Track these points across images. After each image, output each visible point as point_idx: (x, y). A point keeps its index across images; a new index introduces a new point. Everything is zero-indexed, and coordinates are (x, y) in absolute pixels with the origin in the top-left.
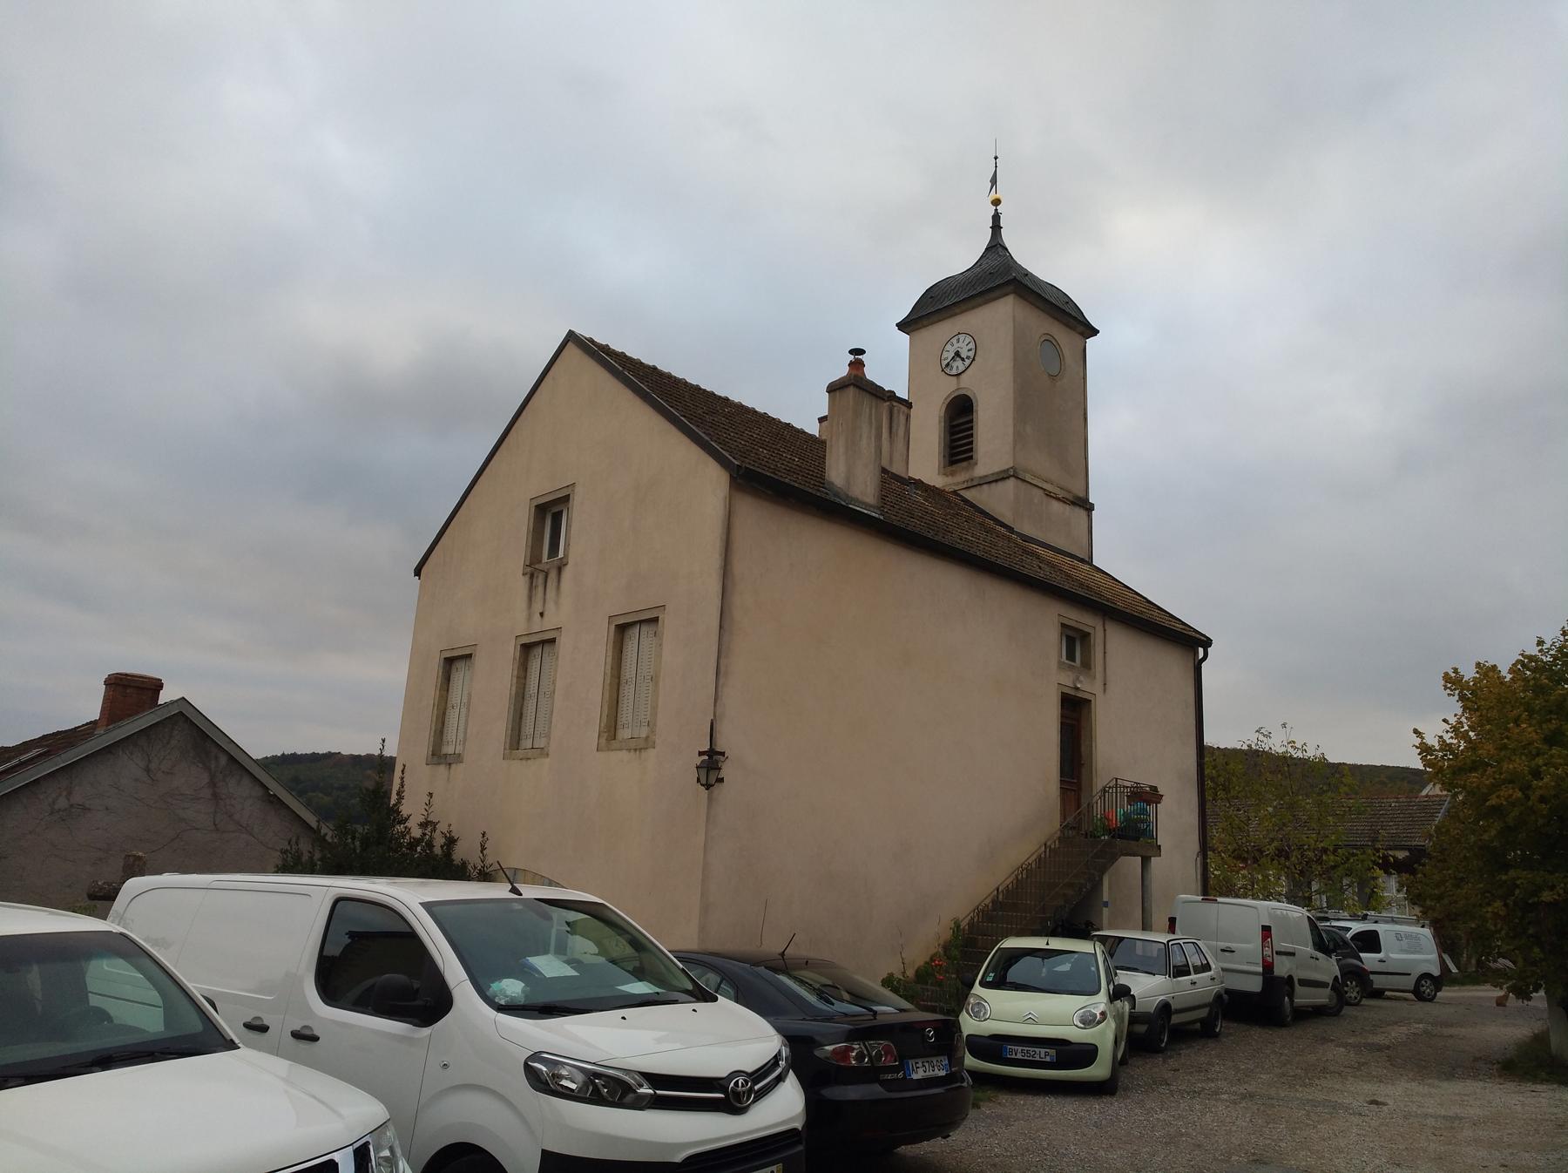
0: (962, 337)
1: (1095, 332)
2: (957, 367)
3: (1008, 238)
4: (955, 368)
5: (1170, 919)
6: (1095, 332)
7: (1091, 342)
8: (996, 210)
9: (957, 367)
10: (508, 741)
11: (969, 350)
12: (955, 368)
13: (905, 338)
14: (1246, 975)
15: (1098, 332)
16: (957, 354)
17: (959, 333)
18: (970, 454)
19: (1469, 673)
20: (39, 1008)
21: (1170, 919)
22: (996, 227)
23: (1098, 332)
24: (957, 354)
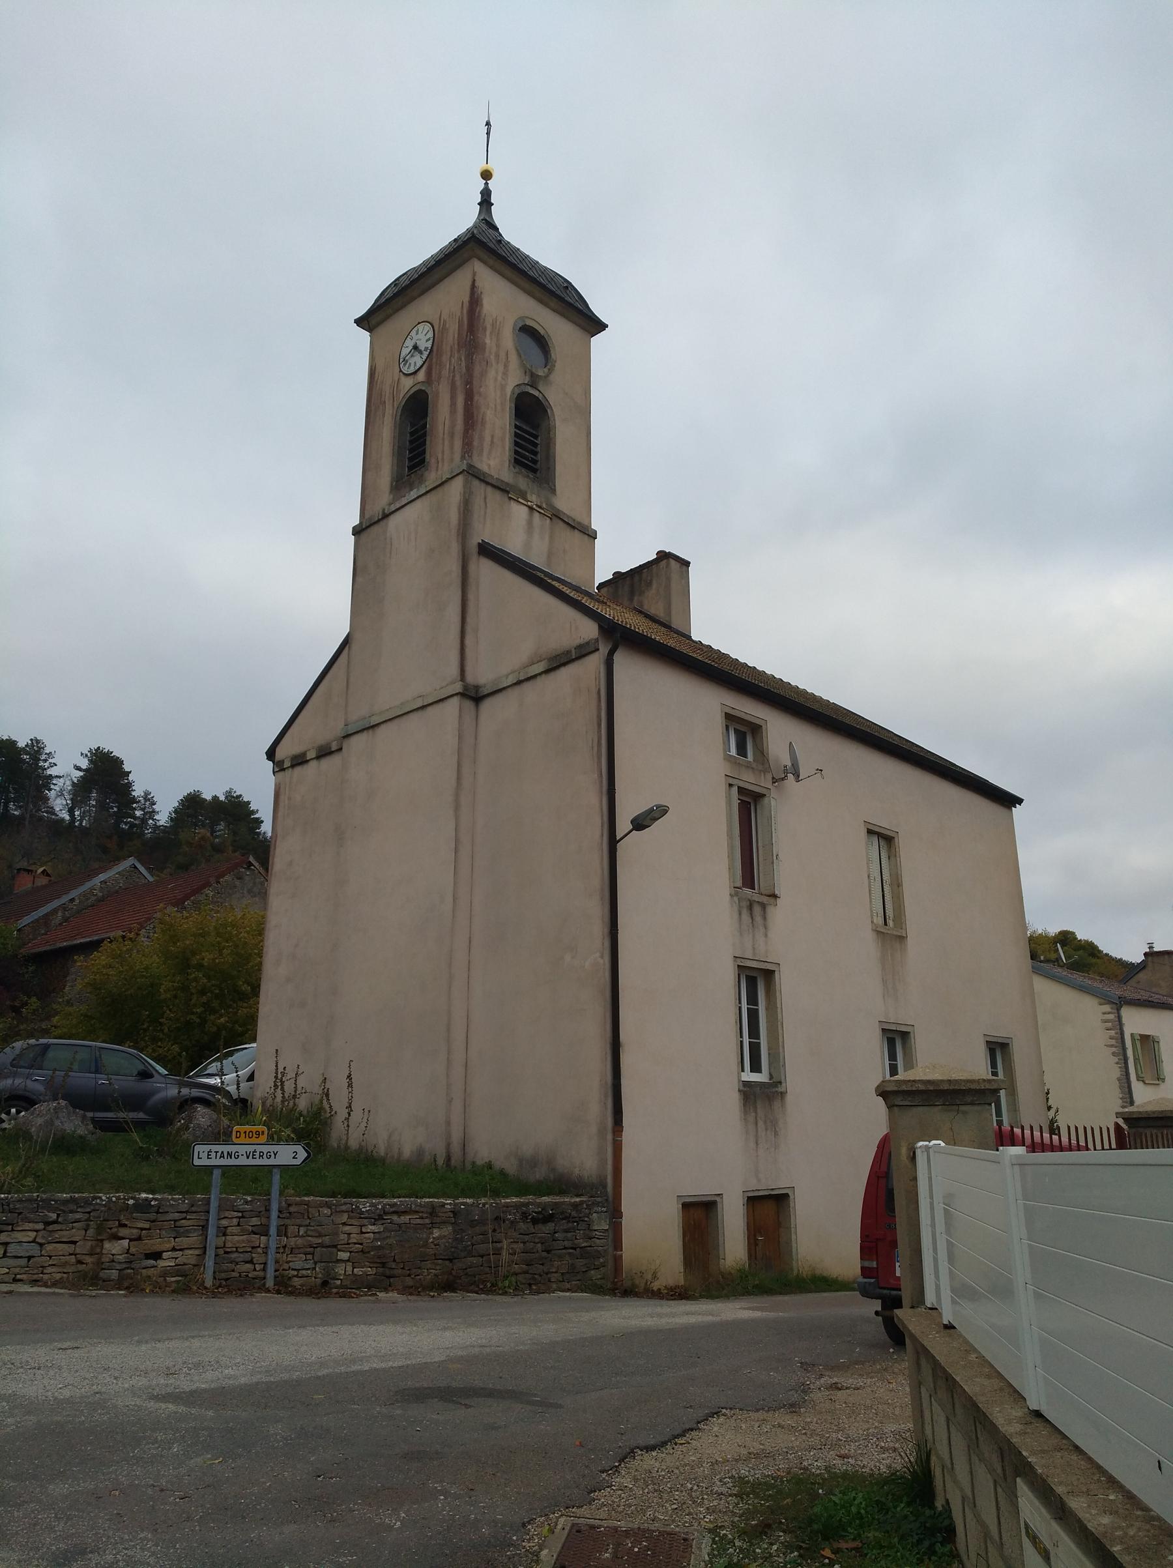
0: (420, 327)
1: (599, 326)
2: (415, 363)
3: (498, 216)
4: (412, 365)
5: (688, 1207)
6: (599, 326)
7: (597, 341)
8: (486, 184)
9: (415, 363)
10: (1013, 1068)
11: (427, 341)
12: (412, 365)
13: (365, 336)
14: (1101, 1163)
15: (607, 326)
16: (415, 347)
17: (419, 323)
18: (1160, 1144)
19: (86, 752)
20: (226, 801)
21: (688, 1207)
22: (486, 202)
23: (607, 326)
24: (415, 347)
